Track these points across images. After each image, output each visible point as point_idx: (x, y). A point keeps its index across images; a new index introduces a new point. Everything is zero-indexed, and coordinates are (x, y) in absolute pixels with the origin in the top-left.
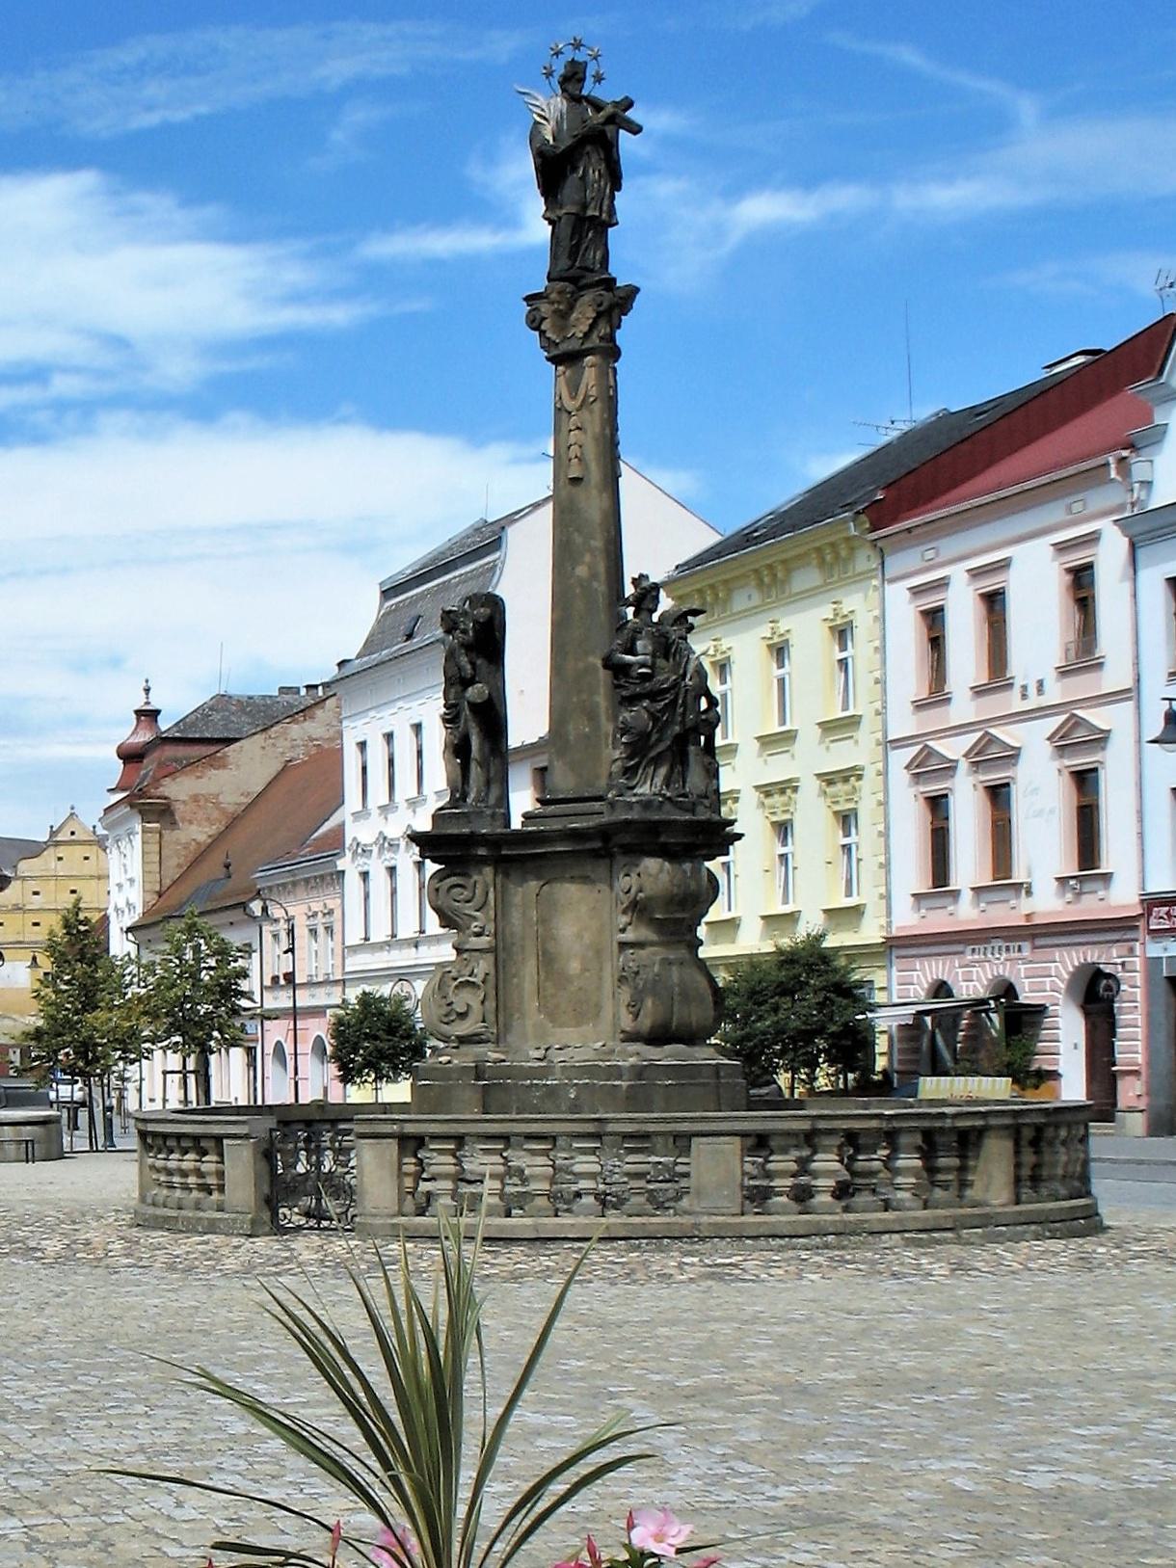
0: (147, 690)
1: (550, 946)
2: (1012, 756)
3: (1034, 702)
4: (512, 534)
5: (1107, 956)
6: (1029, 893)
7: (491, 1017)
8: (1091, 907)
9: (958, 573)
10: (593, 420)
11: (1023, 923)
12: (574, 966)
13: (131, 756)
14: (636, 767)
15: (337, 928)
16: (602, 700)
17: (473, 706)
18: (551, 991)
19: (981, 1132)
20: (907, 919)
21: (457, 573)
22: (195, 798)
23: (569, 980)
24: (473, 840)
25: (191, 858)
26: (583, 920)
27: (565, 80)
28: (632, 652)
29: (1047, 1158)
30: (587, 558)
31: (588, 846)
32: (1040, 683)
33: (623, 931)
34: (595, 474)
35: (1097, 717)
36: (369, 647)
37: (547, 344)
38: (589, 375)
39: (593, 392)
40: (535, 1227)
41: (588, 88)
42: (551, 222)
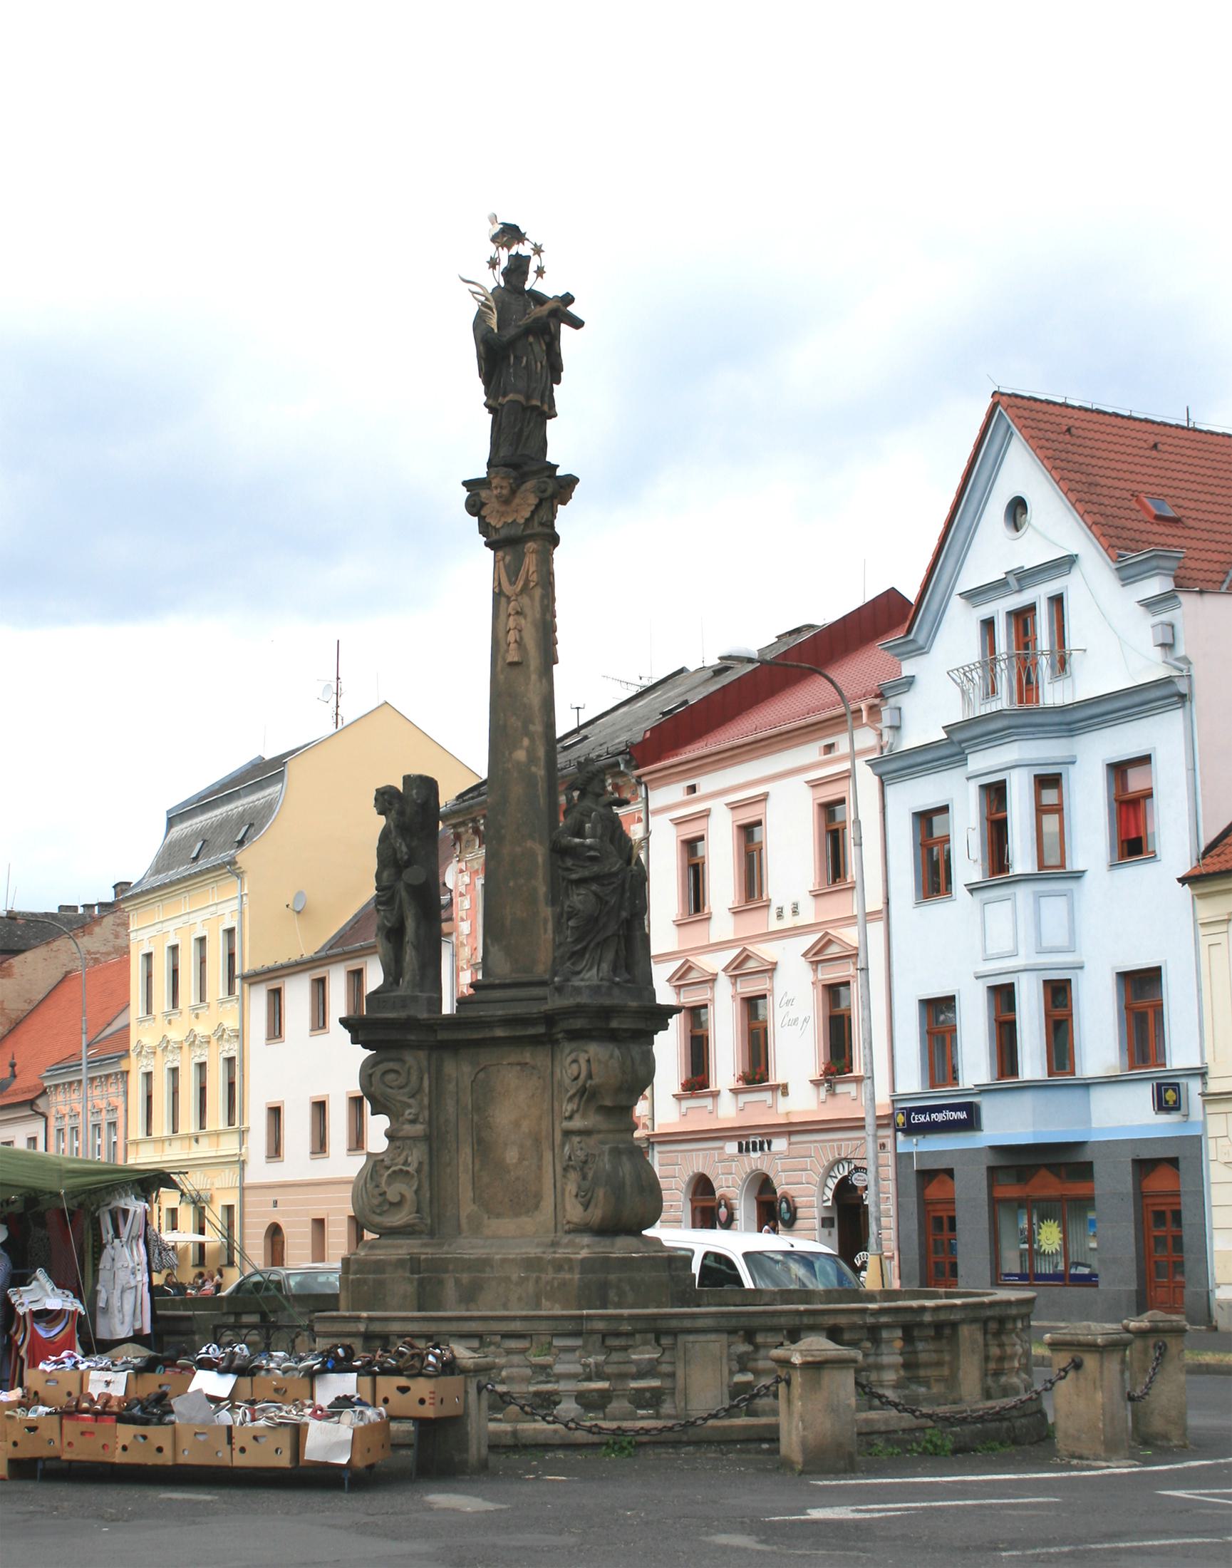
2: (770, 970)
3: (789, 921)
4: (293, 769)
6: (785, 1093)
7: (426, 1209)
9: (718, 808)
10: (532, 606)
12: (511, 1156)
14: (585, 949)
15: (121, 1124)
16: (542, 889)
19: (954, 1325)
24: (410, 1024)
26: (522, 1103)
28: (579, 833)
29: (1009, 1350)
30: (526, 742)
31: (531, 1031)
33: (570, 1118)
34: (534, 661)
35: (850, 935)
36: (158, 868)
37: (484, 529)
38: (530, 563)
39: (534, 577)
40: (515, 1433)
41: (531, 283)
42: (492, 409)
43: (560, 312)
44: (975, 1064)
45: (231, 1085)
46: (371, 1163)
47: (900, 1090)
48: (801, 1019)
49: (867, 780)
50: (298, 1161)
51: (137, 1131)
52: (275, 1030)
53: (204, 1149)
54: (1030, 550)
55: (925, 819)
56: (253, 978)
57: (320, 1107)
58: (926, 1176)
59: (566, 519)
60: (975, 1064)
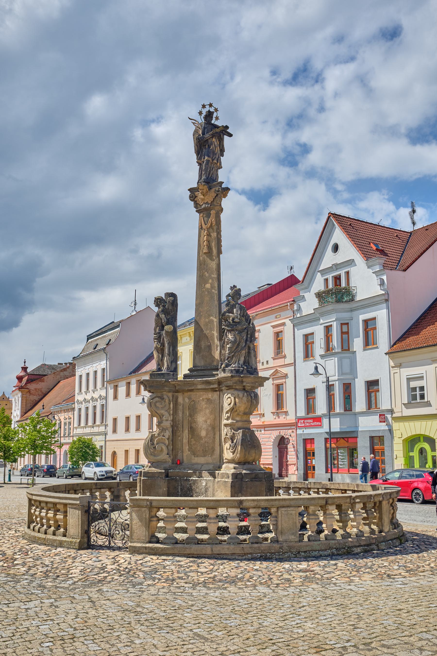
0: (25, 362)
1: (193, 425)
3: (265, 366)
5: (286, 433)
8: (282, 420)
11: (262, 424)
12: (203, 433)
13: (20, 379)
17: (167, 332)
18: (193, 442)
21: (107, 333)
22: (36, 389)
23: (201, 438)
25: (34, 404)
30: (210, 281)
31: (212, 386)
32: (267, 362)
35: (284, 370)
37: (196, 205)
43: (224, 131)
44: (321, 408)
45: (103, 412)
46: (150, 435)
47: (298, 415)
49: (289, 325)
50: (121, 433)
52: (115, 397)
53: (96, 430)
54: (340, 258)
55: (306, 337)
59: (225, 203)
60: (321, 408)
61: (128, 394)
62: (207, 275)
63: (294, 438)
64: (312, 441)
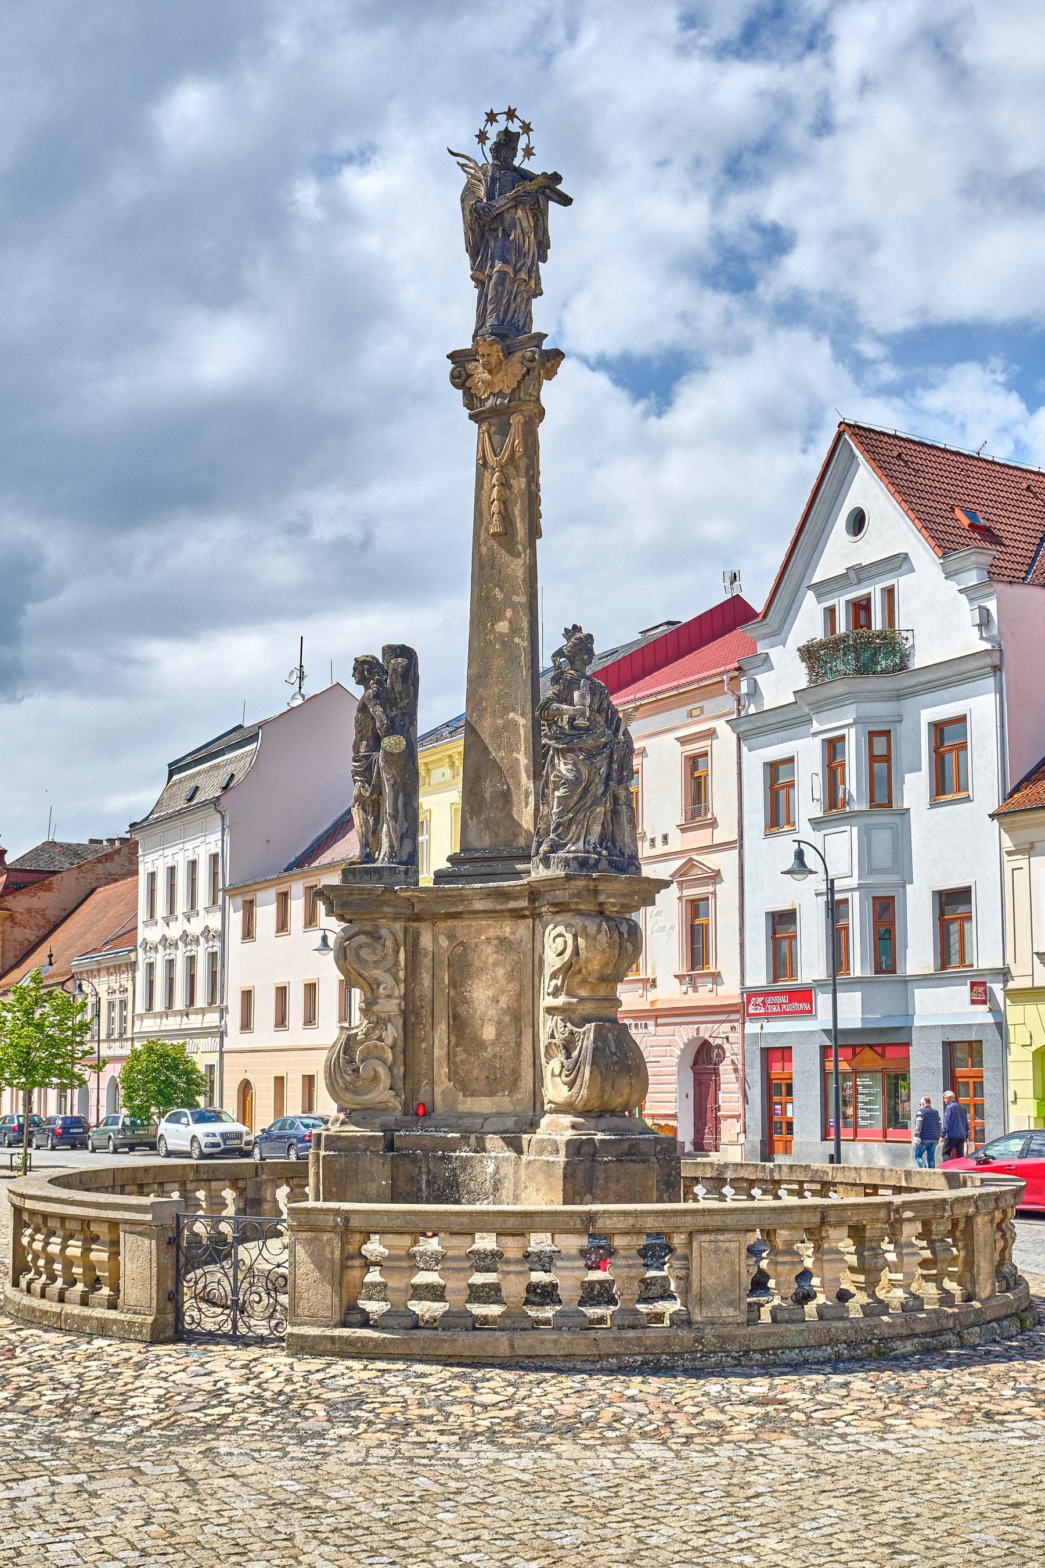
1: (462, 1010)
3: (660, 849)
5: (713, 1031)
8: (704, 996)
11: (649, 1007)
12: (489, 1033)
17: (388, 755)
18: (461, 1056)
20: (670, 992)
22: (29, 911)
23: (482, 1045)
27: (497, 149)
30: (509, 613)
31: (512, 905)
32: (665, 837)
35: (712, 861)
43: (550, 189)
44: (812, 963)
45: (214, 974)
47: (748, 983)
48: (668, 927)
51: (140, 1008)
52: (248, 933)
53: (194, 1021)
54: (869, 549)
55: (773, 768)
56: (231, 891)
57: (282, 992)
58: (768, 1054)
60: (812, 963)
61: (282, 926)
62: (500, 596)
63: (738, 1044)
64: (785, 1053)
